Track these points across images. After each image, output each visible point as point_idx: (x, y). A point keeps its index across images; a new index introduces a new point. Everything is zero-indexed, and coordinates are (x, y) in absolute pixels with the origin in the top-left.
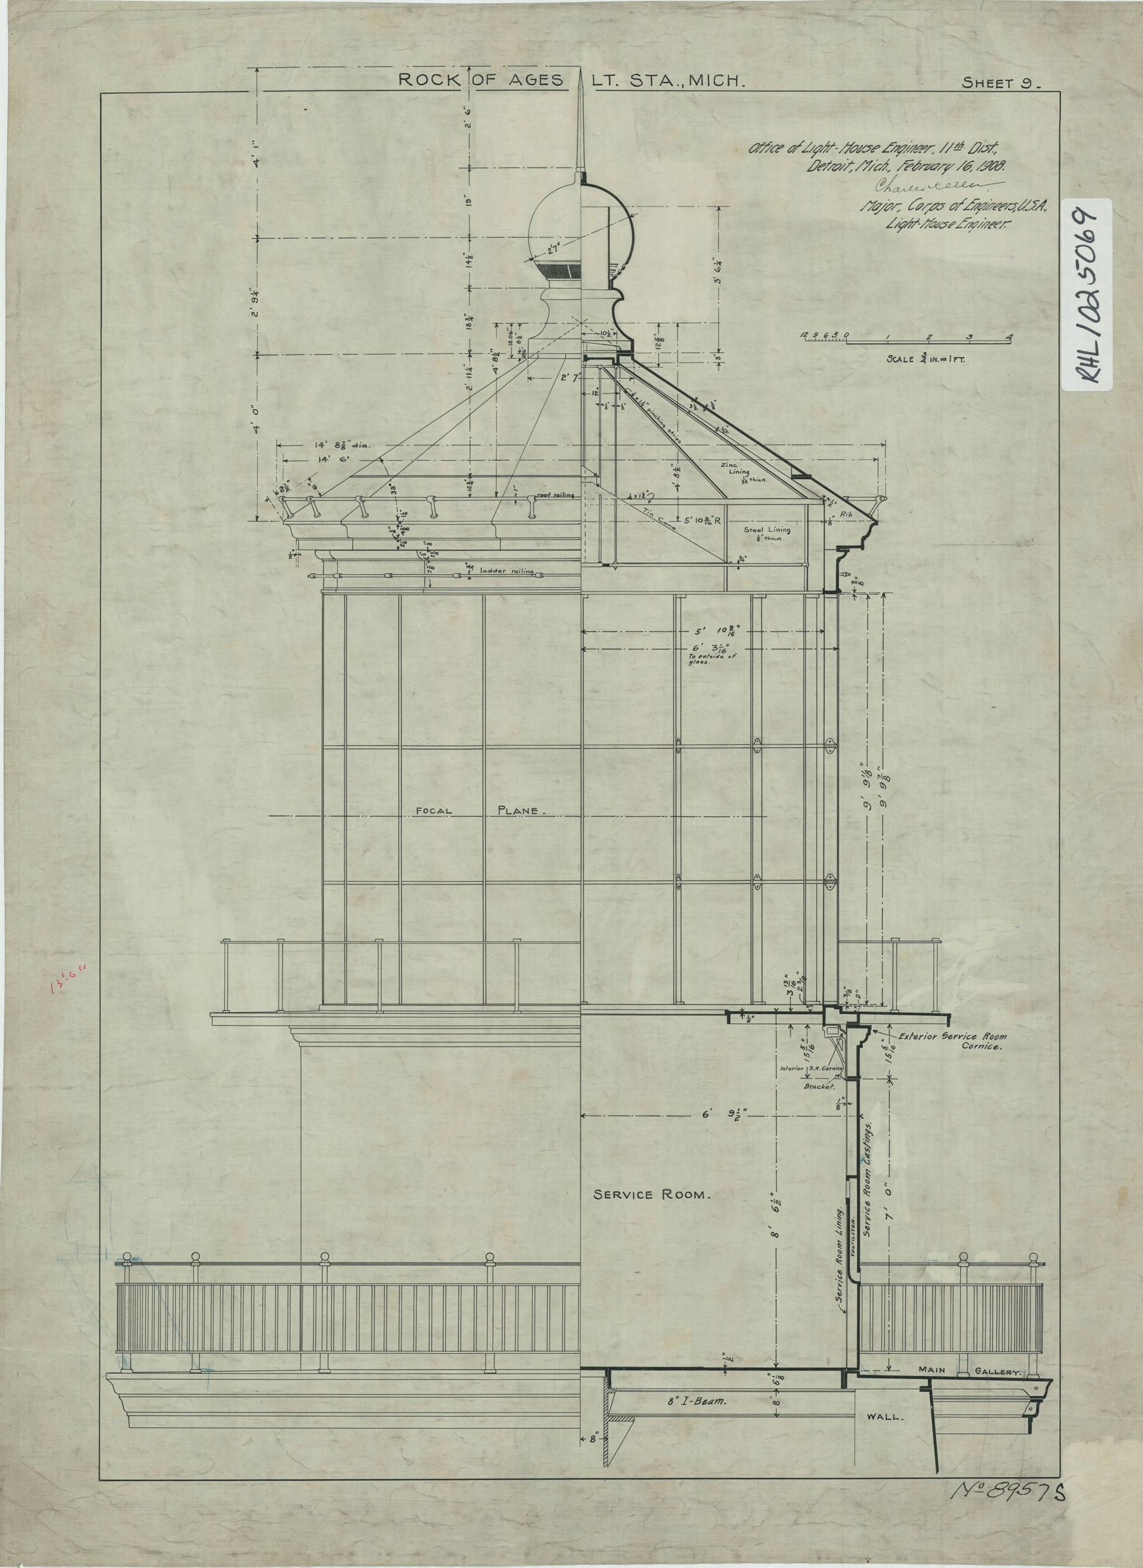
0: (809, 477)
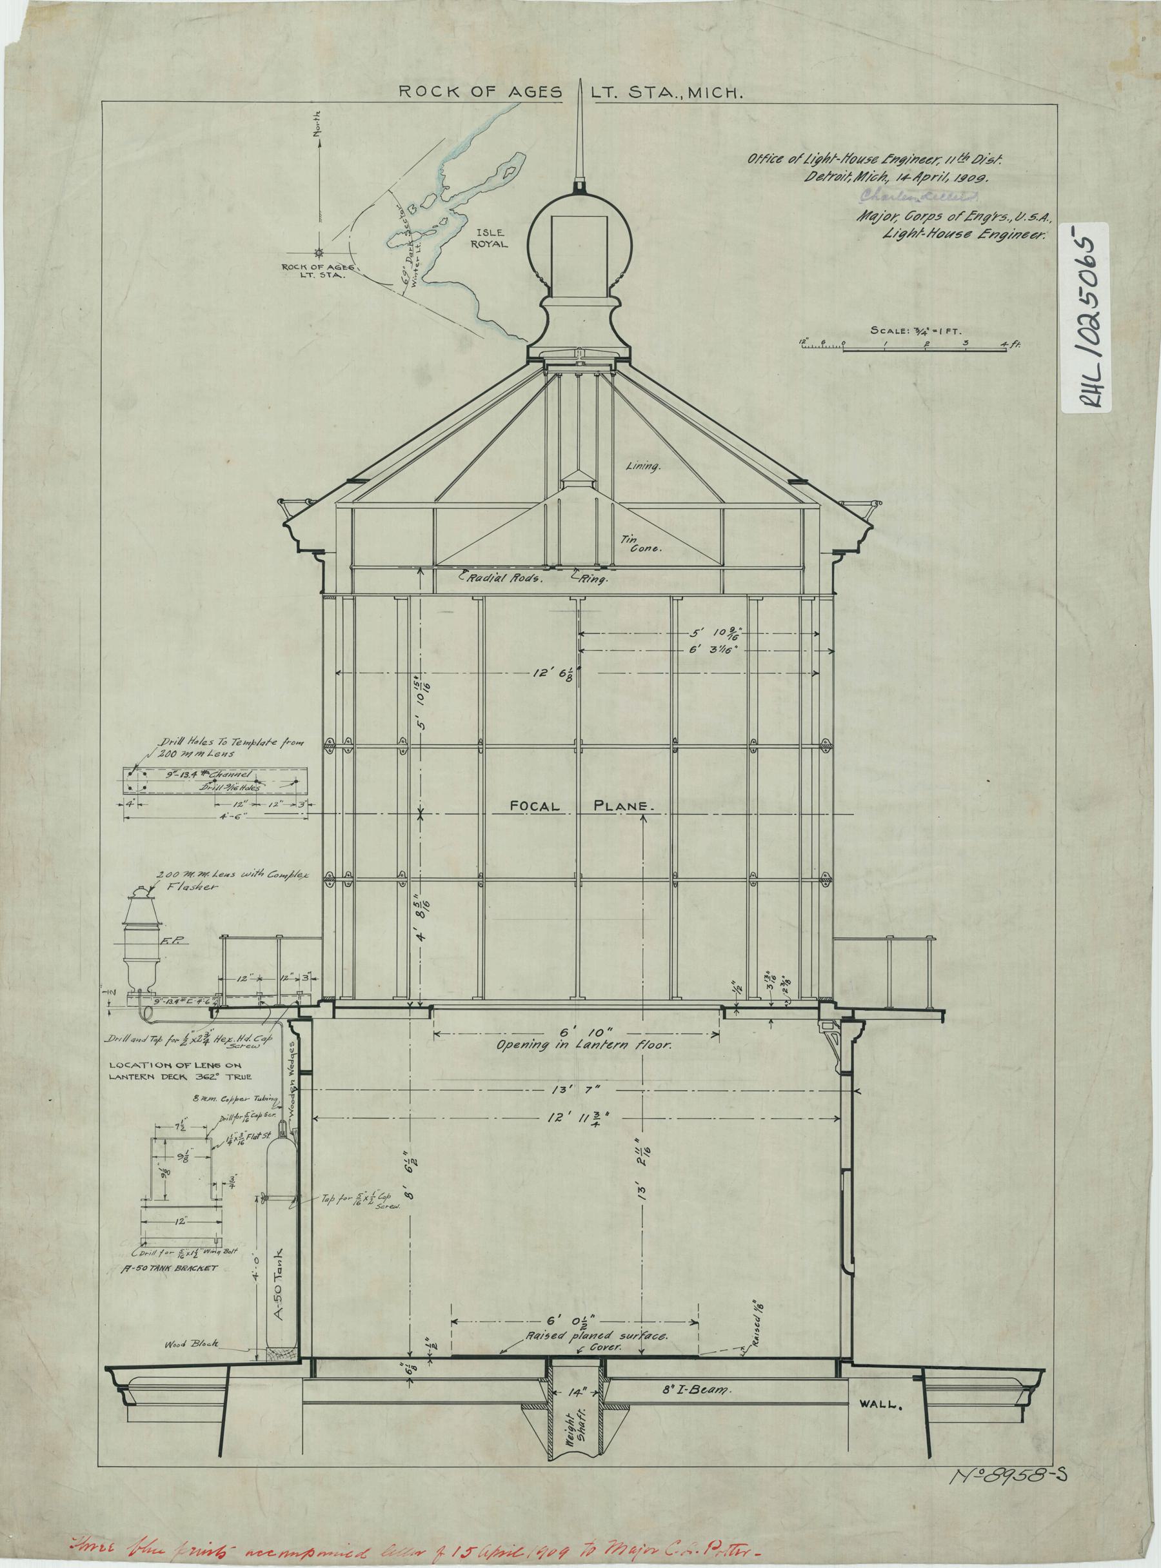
0: (805, 482)
